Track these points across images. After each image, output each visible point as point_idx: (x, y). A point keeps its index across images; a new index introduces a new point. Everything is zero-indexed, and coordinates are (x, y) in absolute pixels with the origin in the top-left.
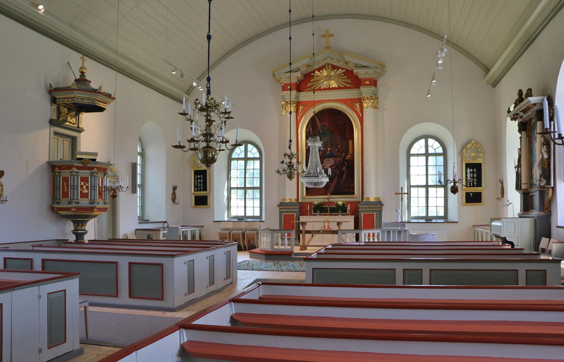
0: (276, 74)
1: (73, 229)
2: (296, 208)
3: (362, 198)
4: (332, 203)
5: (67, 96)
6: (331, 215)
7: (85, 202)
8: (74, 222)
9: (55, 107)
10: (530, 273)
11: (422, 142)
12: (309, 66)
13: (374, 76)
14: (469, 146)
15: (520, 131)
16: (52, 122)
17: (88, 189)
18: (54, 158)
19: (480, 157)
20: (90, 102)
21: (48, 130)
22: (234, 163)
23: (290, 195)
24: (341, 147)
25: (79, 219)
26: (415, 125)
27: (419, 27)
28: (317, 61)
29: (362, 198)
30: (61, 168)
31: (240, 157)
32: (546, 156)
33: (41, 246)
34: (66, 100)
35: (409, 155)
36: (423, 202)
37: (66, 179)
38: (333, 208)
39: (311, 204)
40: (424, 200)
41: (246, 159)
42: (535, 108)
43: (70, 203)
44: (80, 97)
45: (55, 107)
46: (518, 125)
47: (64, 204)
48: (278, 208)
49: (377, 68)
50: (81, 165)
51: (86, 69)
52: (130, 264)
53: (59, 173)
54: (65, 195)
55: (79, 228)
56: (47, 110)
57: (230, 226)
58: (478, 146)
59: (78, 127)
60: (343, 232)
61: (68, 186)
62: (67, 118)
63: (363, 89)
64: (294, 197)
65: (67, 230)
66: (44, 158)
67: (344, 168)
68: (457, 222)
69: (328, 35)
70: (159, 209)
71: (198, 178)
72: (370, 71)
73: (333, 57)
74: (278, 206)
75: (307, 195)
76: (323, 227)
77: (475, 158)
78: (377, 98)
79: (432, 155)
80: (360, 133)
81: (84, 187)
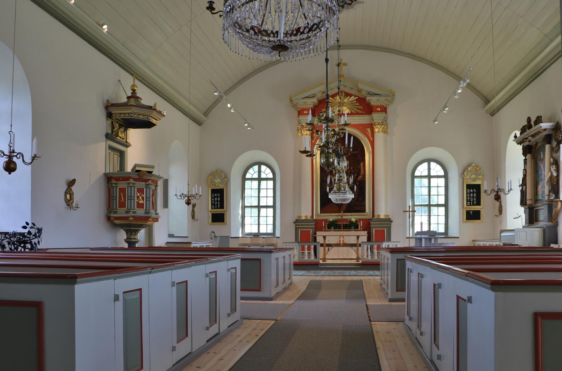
0: (293, 99)
1: (125, 238)
3: (373, 216)
4: (346, 220)
7: (141, 212)
8: (127, 232)
9: (110, 122)
11: (425, 165)
13: (384, 104)
14: (469, 169)
15: (525, 154)
17: (143, 200)
19: (479, 179)
20: (145, 118)
21: (104, 143)
22: (247, 183)
24: (353, 168)
25: (131, 230)
26: (263, 150)
27: (426, 60)
29: (373, 216)
30: (118, 179)
32: (555, 174)
34: (122, 115)
35: (413, 177)
38: (346, 225)
39: (326, 221)
41: (260, 179)
42: (545, 133)
43: (127, 212)
44: (135, 113)
45: (109, 122)
46: (523, 149)
47: (121, 212)
48: (294, 225)
49: (388, 95)
54: (122, 205)
55: (132, 237)
56: (102, 124)
58: (478, 168)
59: (126, 142)
61: (124, 197)
62: (118, 132)
63: (375, 116)
64: (309, 215)
65: (120, 238)
68: (458, 238)
71: (215, 197)
72: (382, 99)
73: (346, 85)
74: (294, 223)
75: (321, 212)
77: (474, 180)
80: (371, 156)
81: (140, 198)
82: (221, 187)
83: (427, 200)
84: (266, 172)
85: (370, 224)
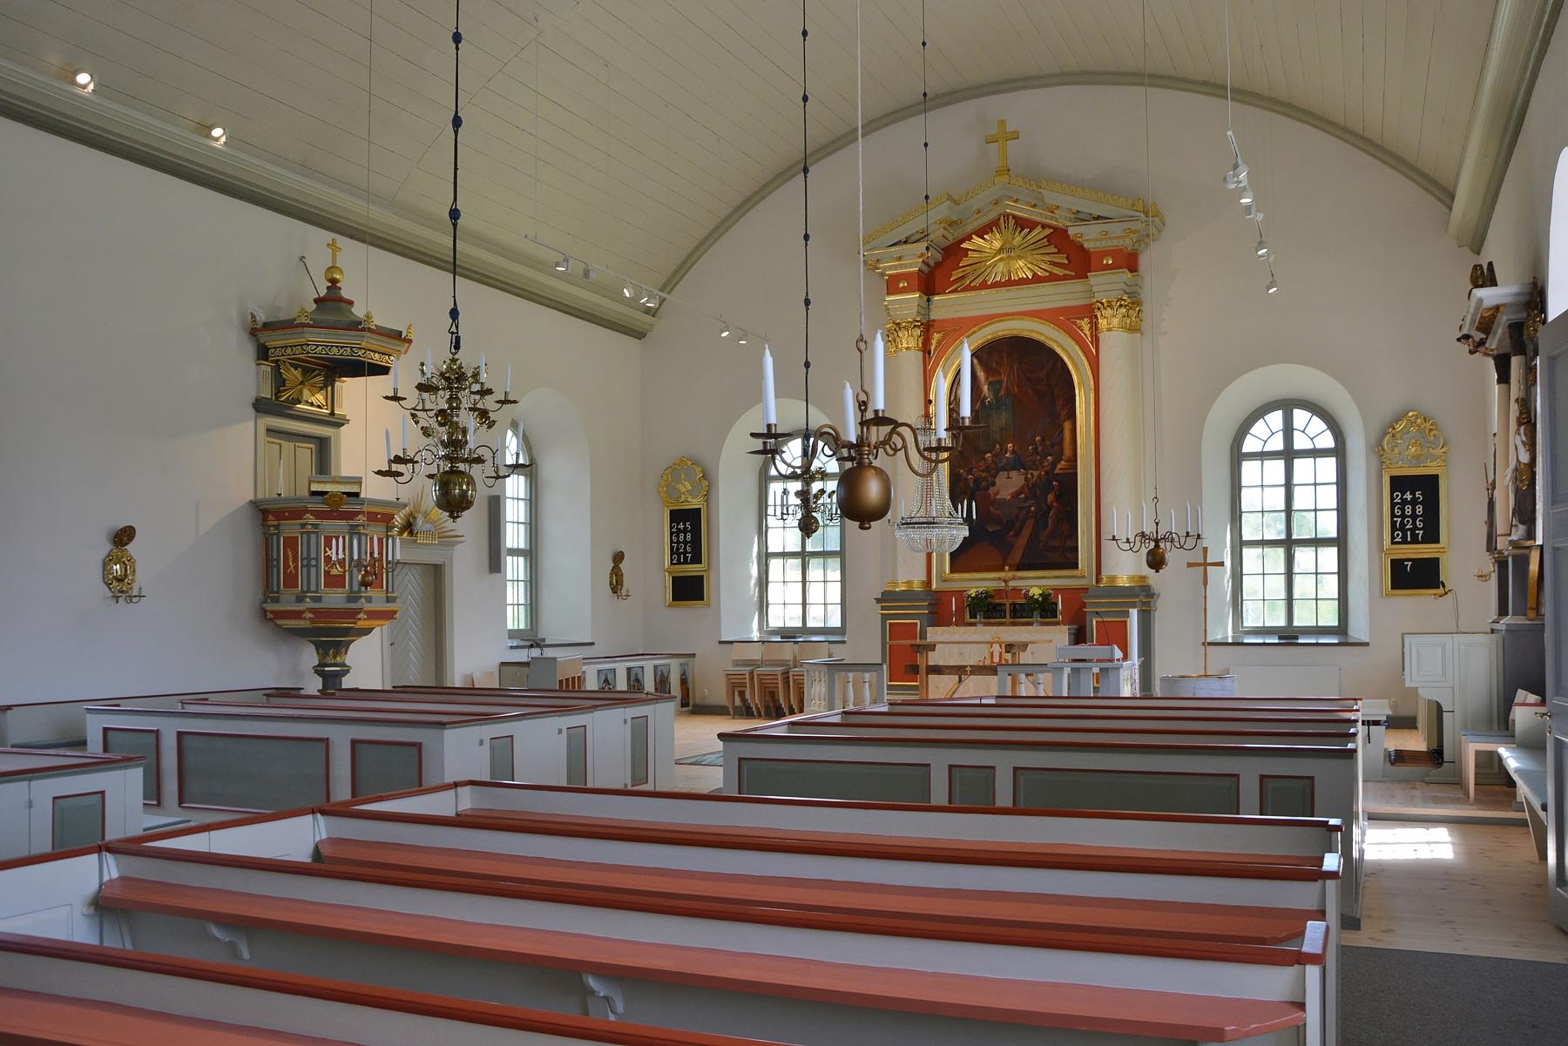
2: (922, 607)
3: (1098, 580)
4: (1016, 590)
5: (282, 343)
6: (1014, 624)
7: (335, 599)
8: (318, 646)
10: (1270, 784)
11: (1276, 419)
12: (952, 224)
13: (1127, 244)
14: (1399, 427)
16: (261, 406)
18: (265, 493)
19: (1435, 458)
20: (346, 354)
21: (251, 424)
22: (1250, 470)
23: (910, 574)
24: (1043, 440)
25: (331, 636)
28: (975, 208)
29: (1098, 580)
31: (1269, 447)
32: (1525, 457)
33: (204, 702)
35: (1237, 457)
36: (1277, 585)
37: (291, 543)
40: (1281, 581)
41: (1289, 454)
43: (300, 599)
44: (323, 343)
45: (267, 368)
47: (287, 603)
49: (1131, 219)
50: (325, 508)
51: (341, 272)
52: (354, 742)
53: (277, 527)
55: (329, 660)
56: (250, 379)
57: (755, 653)
58: (1428, 425)
59: (332, 414)
60: (1029, 670)
61: (295, 560)
62: (301, 392)
63: (1097, 280)
64: (918, 577)
65: (299, 666)
66: (244, 492)
67: (1050, 497)
68: (1367, 644)
69: (1002, 136)
70: (577, 614)
71: (679, 531)
72: (1115, 229)
74: (878, 601)
76: (988, 655)
78: (1139, 303)
79: (1273, 455)
82: (694, 503)
83: (1282, 526)
84: (1311, 431)
85: (1084, 605)
